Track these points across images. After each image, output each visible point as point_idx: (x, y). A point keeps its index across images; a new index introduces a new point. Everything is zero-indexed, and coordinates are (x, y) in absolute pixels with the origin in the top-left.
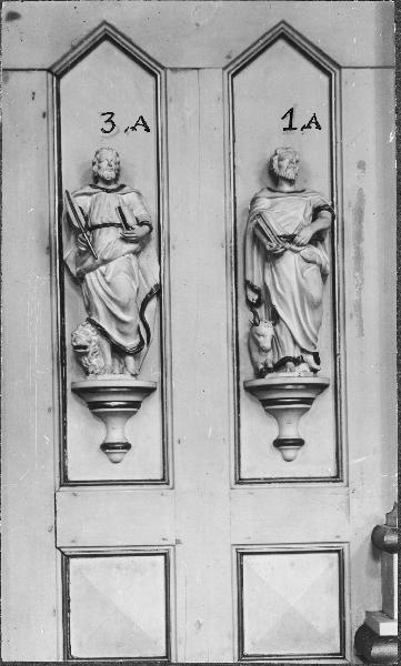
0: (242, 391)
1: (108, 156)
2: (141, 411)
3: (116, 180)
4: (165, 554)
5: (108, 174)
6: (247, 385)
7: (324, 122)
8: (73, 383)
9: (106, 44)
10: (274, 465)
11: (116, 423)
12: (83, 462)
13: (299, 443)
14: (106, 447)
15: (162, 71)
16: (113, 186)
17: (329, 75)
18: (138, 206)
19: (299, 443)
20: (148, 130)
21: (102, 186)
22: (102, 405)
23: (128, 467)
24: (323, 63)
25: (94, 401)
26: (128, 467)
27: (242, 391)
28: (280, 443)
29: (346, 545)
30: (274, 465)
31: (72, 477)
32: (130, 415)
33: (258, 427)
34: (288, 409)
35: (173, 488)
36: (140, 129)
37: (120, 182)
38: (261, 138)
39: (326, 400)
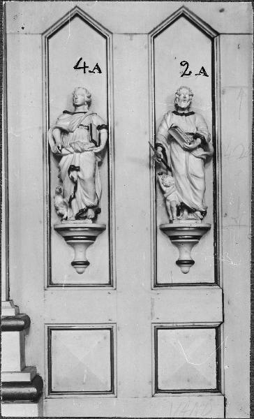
0: (53, 231)
1: (184, 91)
2: (201, 241)
3: (188, 108)
4: (110, 329)
5: (184, 105)
6: (56, 227)
7: (103, 68)
8: (54, 225)
9: (77, 19)
10: (178, 275)
11: (185, 248)
12: (63, 273)
13: (191, 263)
14: (179, 263)
15: (110, 35)
16: (186, 112)
17: (105, 37)
18: (198, 123)
19: (191, 263)
20: (100, 72)
21: (182, 112)
22: (177, 237)
23: (88, 276)
24: (213, 35)
25: (173, 234)
26: (88, 276)
27: (159, 231)
28: (179, 263)
29: (114, 325)
30: (178, 275)
31: (54, 281)
32: (88, 245)
33: (63, 253)
34: (182, 242)
35: (115, 289)
36: (96, 71)
37: (191, 111)
38: (170, 83)
39: (209, 237)
